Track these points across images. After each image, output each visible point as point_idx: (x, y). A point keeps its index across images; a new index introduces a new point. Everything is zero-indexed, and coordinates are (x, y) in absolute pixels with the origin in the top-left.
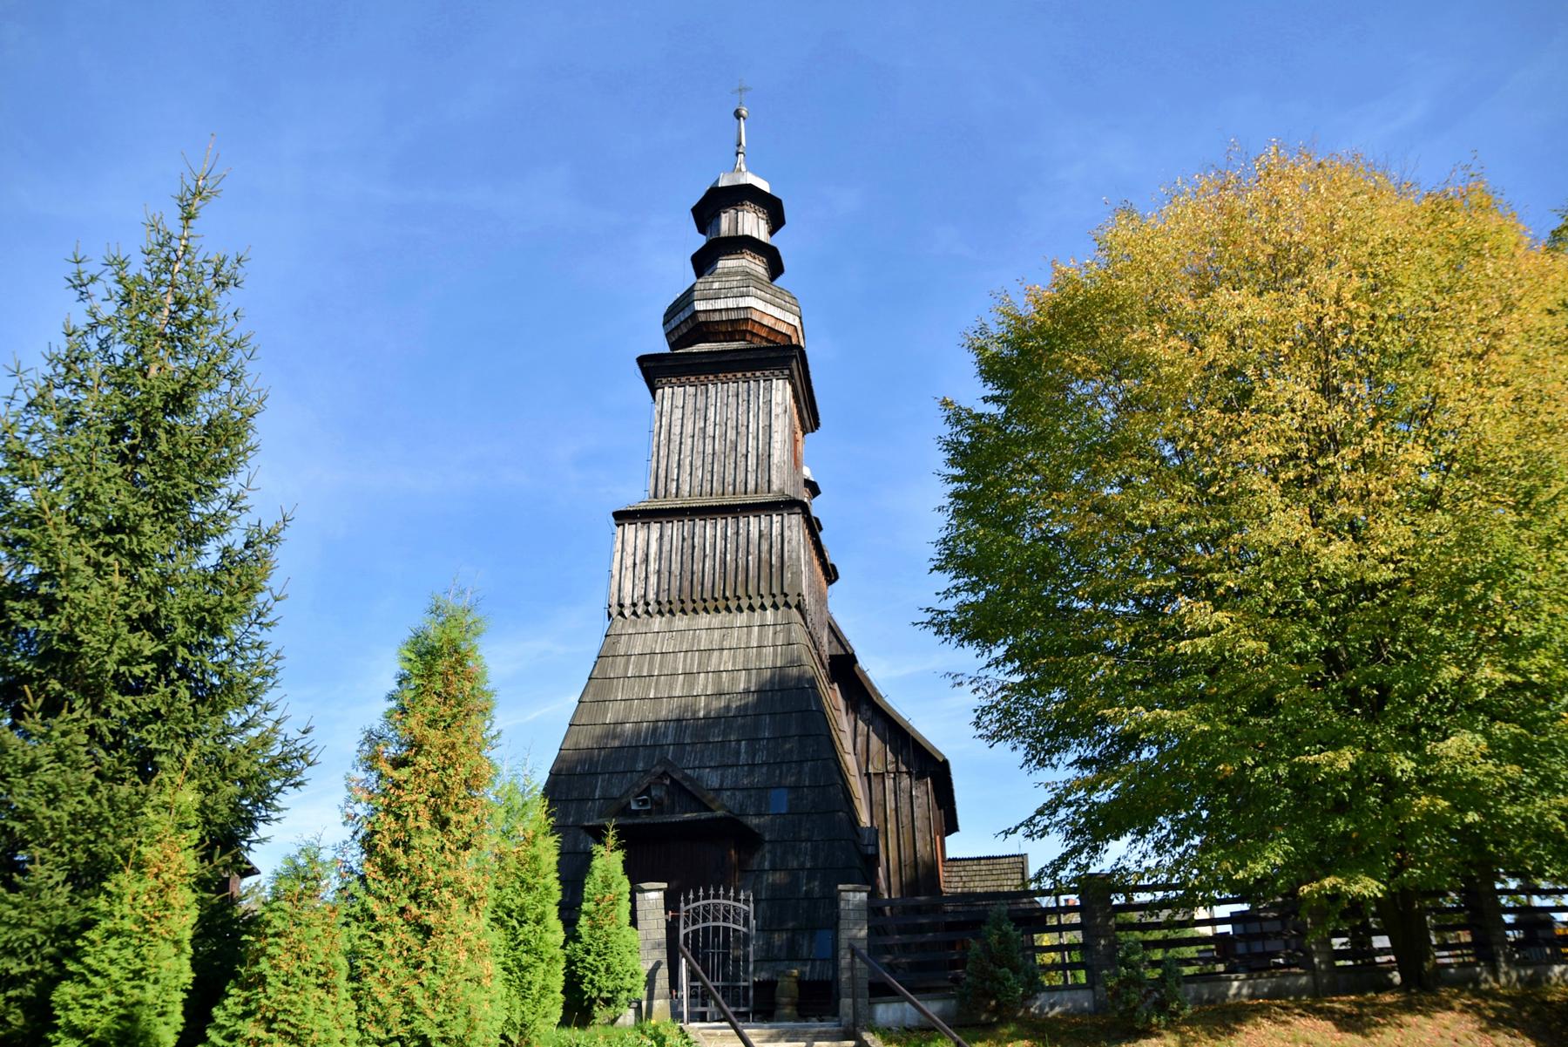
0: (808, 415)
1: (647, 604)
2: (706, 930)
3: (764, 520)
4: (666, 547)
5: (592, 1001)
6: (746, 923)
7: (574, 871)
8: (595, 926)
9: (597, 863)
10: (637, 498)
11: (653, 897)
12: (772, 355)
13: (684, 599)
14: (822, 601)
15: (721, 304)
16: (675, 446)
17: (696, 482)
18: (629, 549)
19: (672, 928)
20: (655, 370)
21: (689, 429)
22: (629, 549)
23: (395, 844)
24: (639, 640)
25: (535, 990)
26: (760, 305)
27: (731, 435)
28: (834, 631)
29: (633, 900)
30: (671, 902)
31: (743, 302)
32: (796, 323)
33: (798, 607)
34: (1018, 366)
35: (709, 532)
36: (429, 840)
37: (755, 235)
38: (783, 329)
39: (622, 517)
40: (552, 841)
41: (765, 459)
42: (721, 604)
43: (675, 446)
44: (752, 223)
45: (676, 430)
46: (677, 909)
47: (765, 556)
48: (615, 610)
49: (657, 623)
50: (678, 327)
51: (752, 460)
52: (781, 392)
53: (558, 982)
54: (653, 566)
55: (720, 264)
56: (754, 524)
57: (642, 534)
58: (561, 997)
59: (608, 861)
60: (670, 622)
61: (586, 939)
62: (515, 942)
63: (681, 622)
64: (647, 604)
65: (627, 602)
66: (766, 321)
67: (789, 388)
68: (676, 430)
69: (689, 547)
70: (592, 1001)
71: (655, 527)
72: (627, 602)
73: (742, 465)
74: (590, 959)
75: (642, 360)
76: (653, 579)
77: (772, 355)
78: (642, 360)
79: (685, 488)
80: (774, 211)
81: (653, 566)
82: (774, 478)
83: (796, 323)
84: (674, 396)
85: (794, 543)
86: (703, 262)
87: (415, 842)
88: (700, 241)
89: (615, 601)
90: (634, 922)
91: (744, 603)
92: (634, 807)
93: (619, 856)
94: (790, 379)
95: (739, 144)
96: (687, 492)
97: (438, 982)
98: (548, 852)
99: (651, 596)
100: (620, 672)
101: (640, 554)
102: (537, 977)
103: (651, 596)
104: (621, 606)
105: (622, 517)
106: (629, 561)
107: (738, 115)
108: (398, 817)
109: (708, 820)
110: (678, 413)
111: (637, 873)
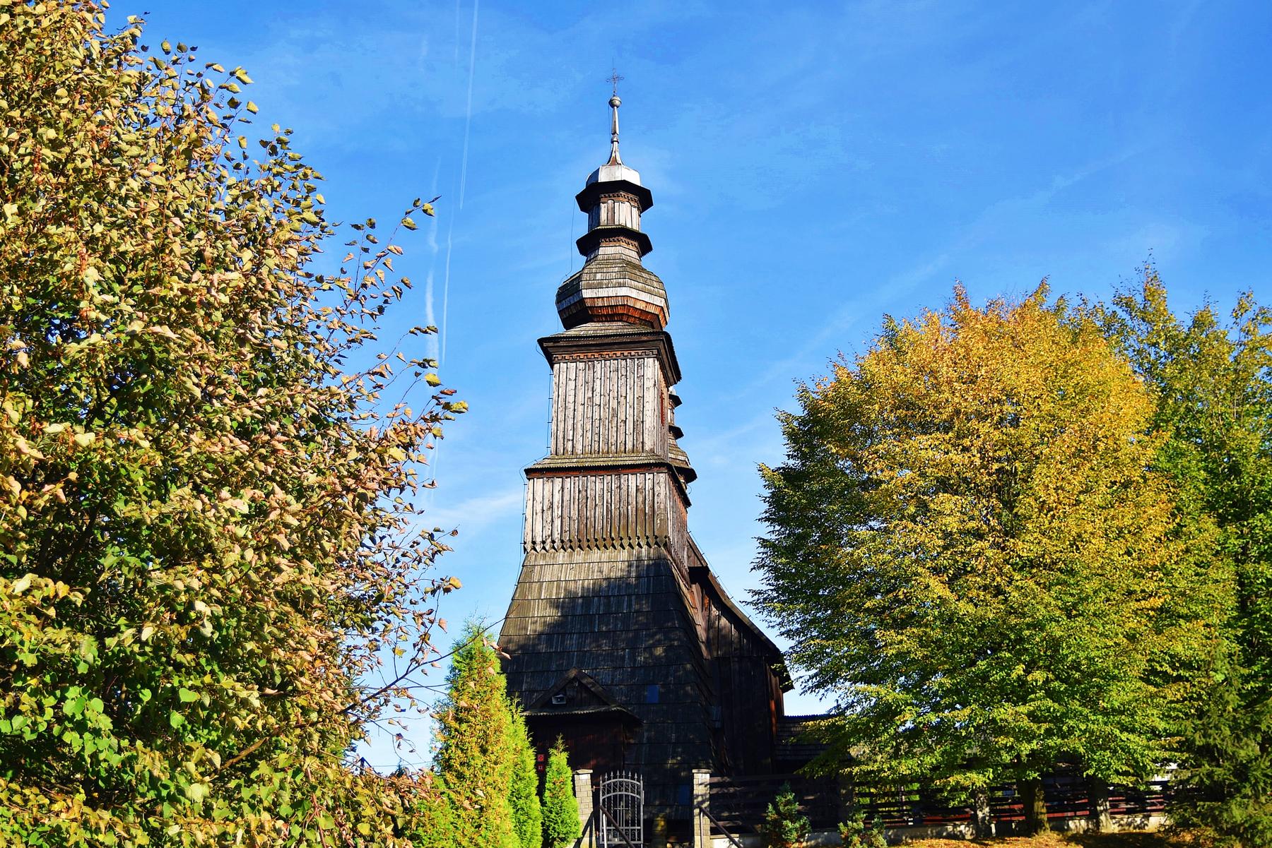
0: (672, 372)
1: (553, 542)
2: (615, 796)
3: (640, 477)
4: (566, 497)
5: (554, 839)
6: (639, 793)
7: (542, 767)
8: (554, 796)
9: (553, 759)
10: (539, 455)
11: (584, 777)
12: (645, 338)
13: (581, 540)
14: (682, 526)
15: (603, 293)
16: (570, 413)
17: (587, 442)
18: (539, 498)
19: (595, 796)
20: (551, 349)
21: (580, 399)
22: (539, 498)
23: (462, 764)
24: (548, 570)
25: (528, 835)
26: (634, 294)
27: (614, 404)
28: (693, 548)
29: (573, 780)
30: (594, 782)
31: (623, 291)
32: (663, 304)
33: (665, 545)
34: (814, 430)
35: (598, 485)
36: (479, 760)
37: (629, 226)
38: (652, 310)
39: (531, 473)
40: (531, 752)
41: (639, 424)
42: (608, 543)
43: (570, 413)
44: (625, 213)
45: (571, 399)
46: (598, 785)
47: (641, 506)
48: (529, 546)
49: (561, 556)
50: (568, 308)
51: (630, 425)
52: (651, 368)
53: (539, 831)
54: (557, 512)
55: (602, 251)
56: (632, 481)
57: (548, 486)
58: (541, 839)
59: (559, 758)
60: (571, 555)
61: (549, 804)
62: (517, 810)
63: (579, 556)
64: (553, 542)
65: (539, 540)
66: (639, 305)
67: (657, 363)
68: (571, 399)
69: (584, 499)
70: (554, 839)
71: (558, 481)
72: (539, 540)
73: (622, 430)
74: (553, 816)
75: (541, 341)
76: (557, 522)
77: (645, 338)
78: (541, 341)
79: (579, 447)
80: (643, 199)
81: (557, 512)
82: (646, 440)
83: (663, 304)
84: (568, 370)
85: (662, 496)
86: (588, 245)
87: (472, 762)
88: (583, 230)
89: (529, 539)
90: (575, 795)
91: (626, 543)
92: (554, 702)
93: (564, 756)
94: (658, 357)
95: (614, 133)
96: (581, 446)
97: (489, 834)
98: (530, 757)
99: (556, 536)
100: (535, 595)
101: (547, 504)
102: (528, 828)
103: (556, 536)
104: (534, 543)
105: (531, 473)
106: (539, 508)
107: (612, 104)
108: (462, 750)
109: (605, 712)
110: (572, 384)
111: (575, 764)
